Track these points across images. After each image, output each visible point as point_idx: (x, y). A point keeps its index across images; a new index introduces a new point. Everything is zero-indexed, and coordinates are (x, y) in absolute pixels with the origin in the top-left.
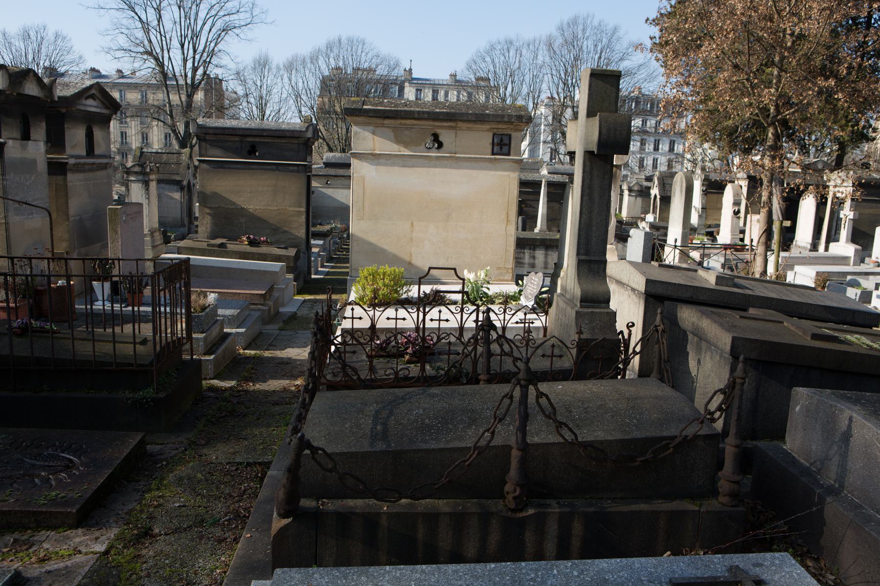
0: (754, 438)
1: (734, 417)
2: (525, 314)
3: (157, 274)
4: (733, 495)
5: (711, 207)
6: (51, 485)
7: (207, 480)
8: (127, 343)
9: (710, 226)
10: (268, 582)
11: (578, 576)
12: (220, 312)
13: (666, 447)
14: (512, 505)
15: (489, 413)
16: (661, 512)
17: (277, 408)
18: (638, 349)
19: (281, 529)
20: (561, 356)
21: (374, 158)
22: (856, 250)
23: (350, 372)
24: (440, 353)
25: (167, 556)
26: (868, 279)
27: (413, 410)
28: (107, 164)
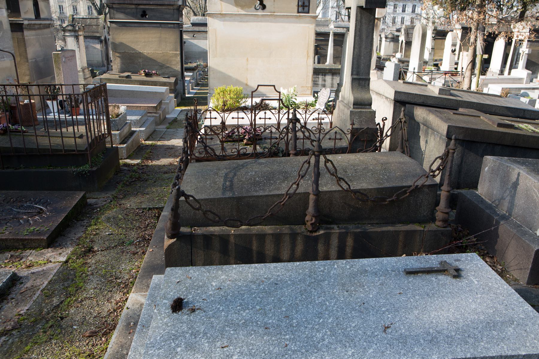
0: (458, 188)
1: (447, 174)
2: (319, 114)
3: (85, 93)
4: (445, 221)
5: (437, 49)
6: (30, 224)
7: (125, 219)
8: (70, 137)
9: (436, 61)
10: (163, 276)
11: (349, 269)
12: (129, 118)
13: (405, 192)
14: (310, 229)
15: (296, 174)
16: (400, 231)
17: (166, 175)
18: (389, 133)
19: (170, 245)
20: (341, 139)
21: (222, 16)
22: (528, 74)
23: (209, 150)
24: (265, 139)
25: (103, 263)
26: (534, 92)
27: (249, 172)
28: (50, 24)
